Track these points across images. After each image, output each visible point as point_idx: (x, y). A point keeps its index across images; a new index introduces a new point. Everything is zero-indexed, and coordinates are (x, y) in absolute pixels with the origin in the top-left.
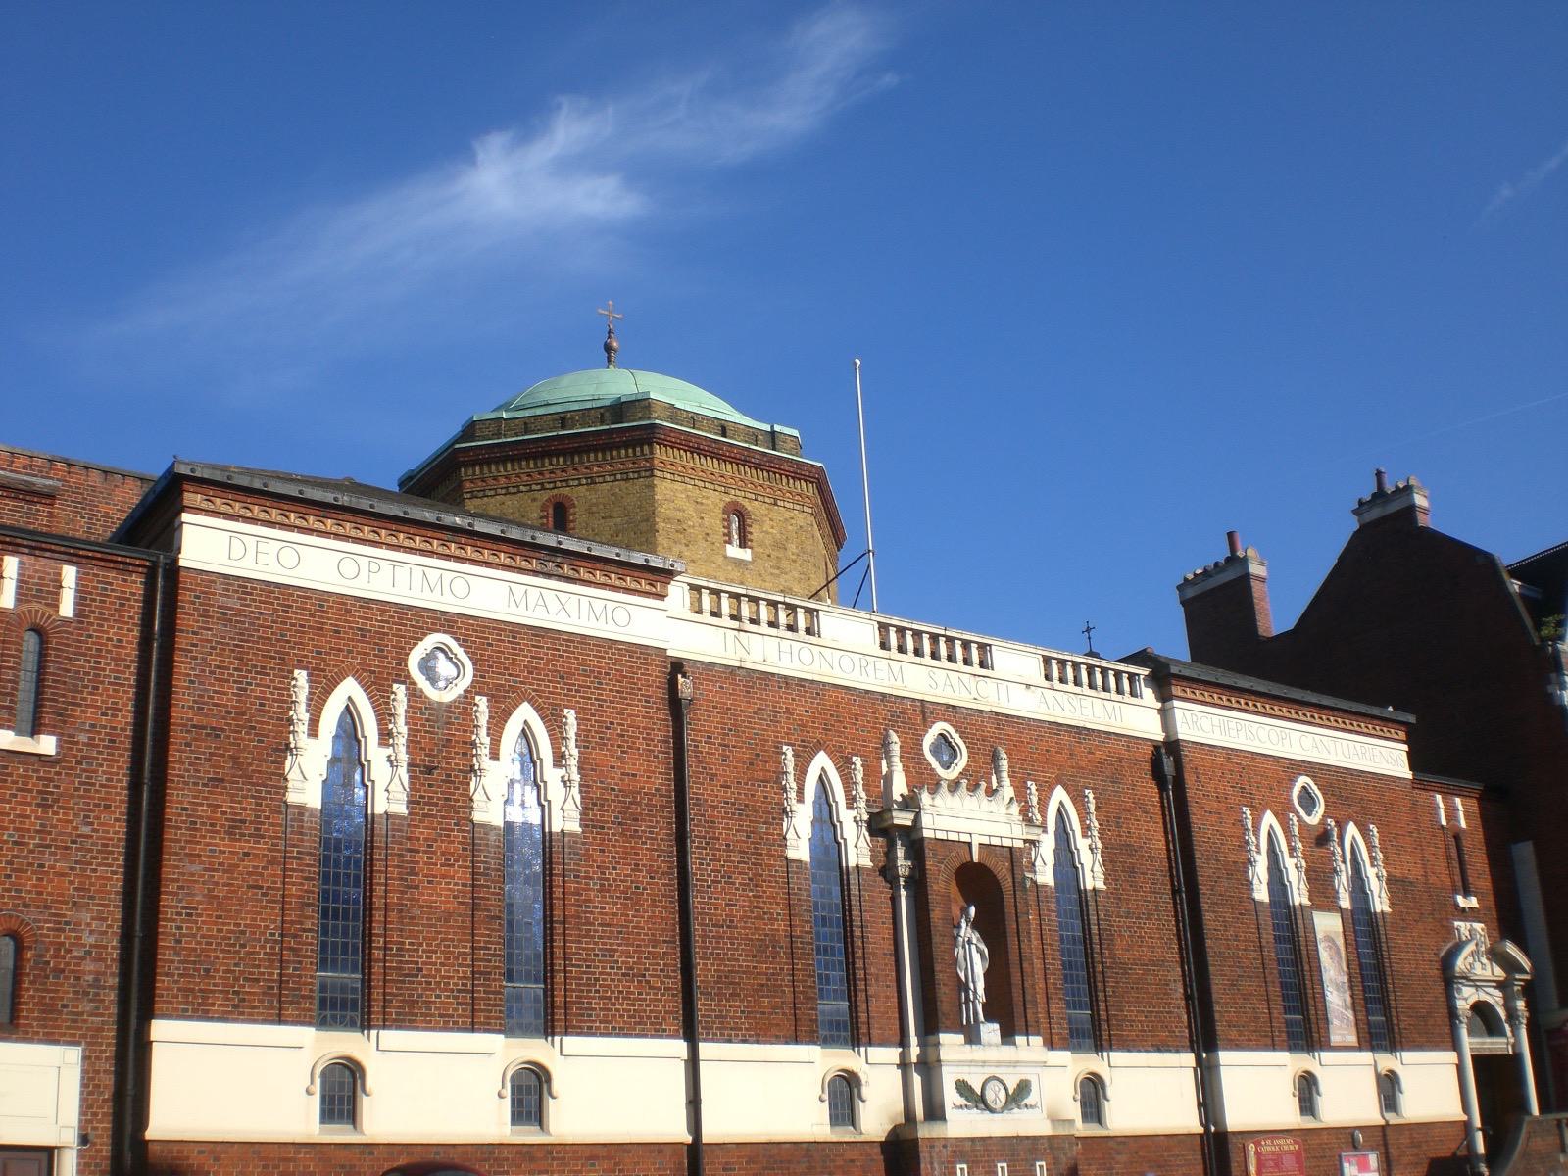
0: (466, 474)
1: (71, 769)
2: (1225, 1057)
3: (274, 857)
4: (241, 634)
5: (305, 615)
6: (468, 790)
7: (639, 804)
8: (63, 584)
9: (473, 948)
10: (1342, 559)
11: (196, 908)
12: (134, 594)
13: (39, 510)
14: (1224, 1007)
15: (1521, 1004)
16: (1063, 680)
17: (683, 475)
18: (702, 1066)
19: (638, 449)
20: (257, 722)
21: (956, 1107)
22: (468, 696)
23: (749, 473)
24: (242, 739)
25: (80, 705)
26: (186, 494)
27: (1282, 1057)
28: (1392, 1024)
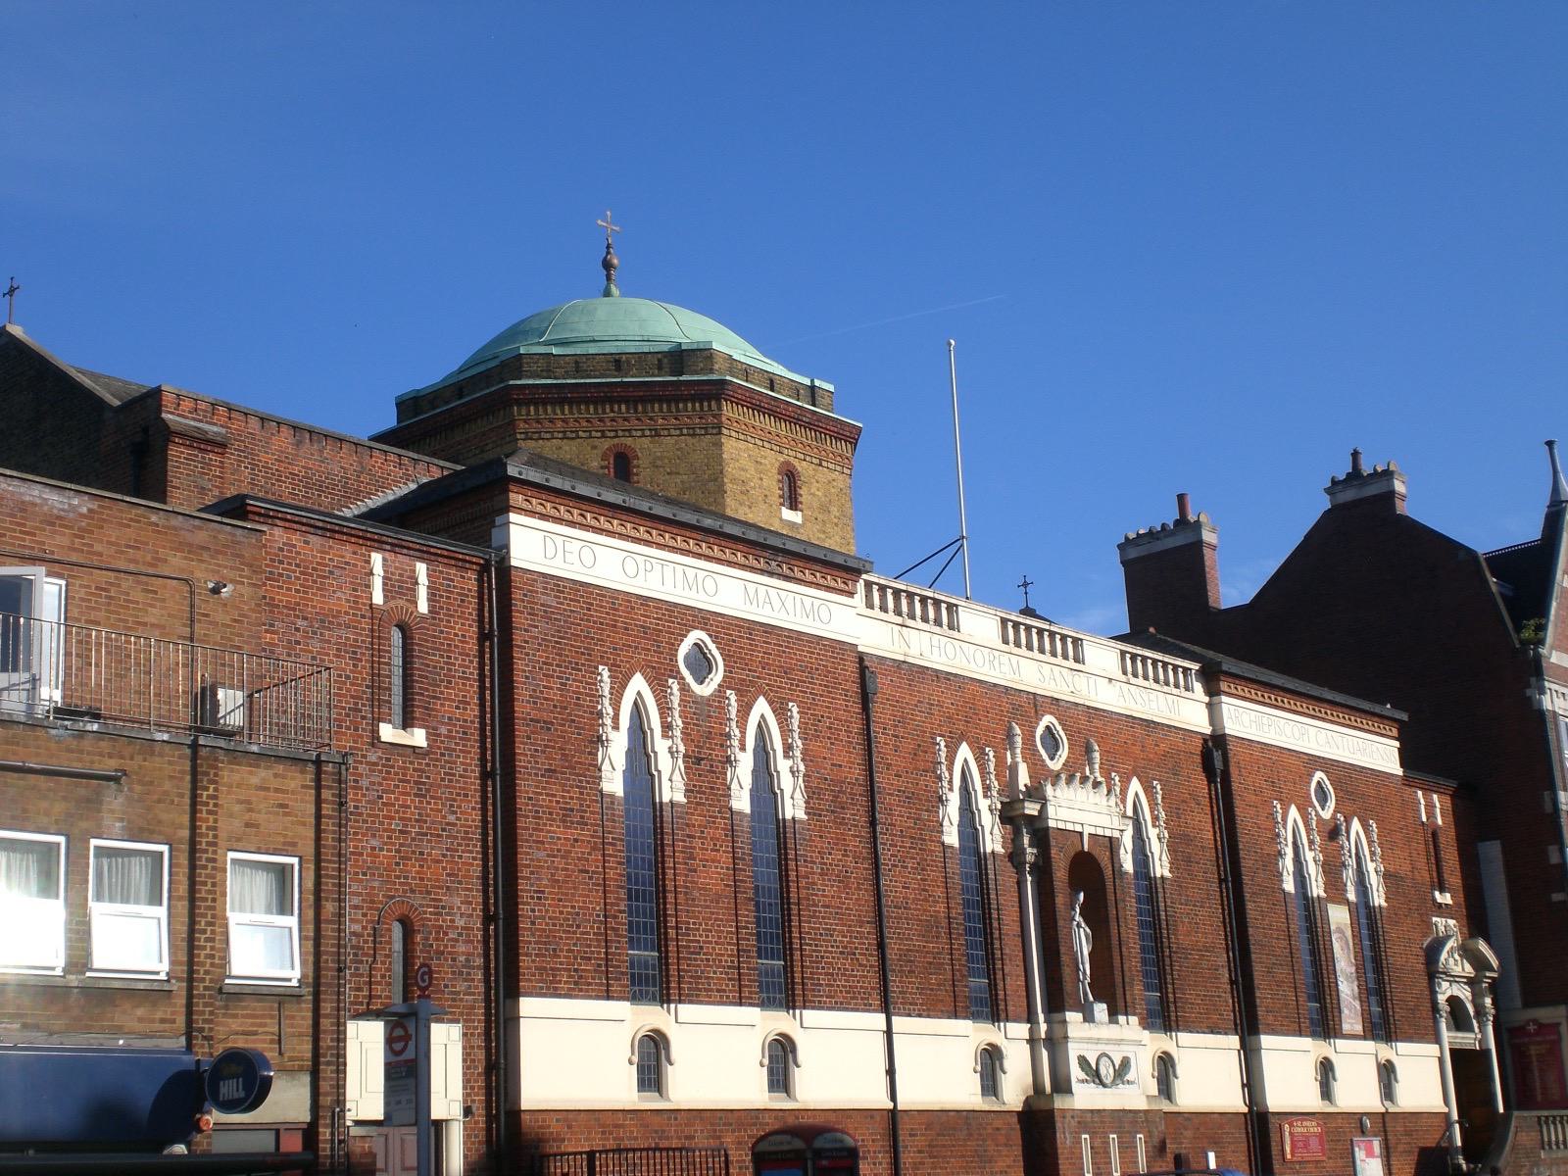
0: (520, 414)
1: (437, 760)
2: (1267, 1041)
3: (595, 843)
4: (559, 631)
5: (602, 612)
6: (725, 779)
7: (844, 793)
8: (374, 571)
9: (737, 927)
11: (543, 892)
12: (470, 590)
13: (211, 459)
14: (1263, 995)
15: (1488, 1001)
16: (1135, 675)
17: (746, 432)
19: (706, 404)
20: (576, 715)
21: (1082, 1081)
23: (801, 434)
24: (566, 732)
25: (439, 698)
26: (511, 494)
27: (1306, 1042)
28: (1388, 1016)
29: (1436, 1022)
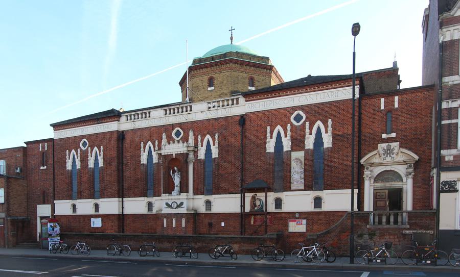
18: (246, 198)
22: (88, 148)
23: (214, 68)
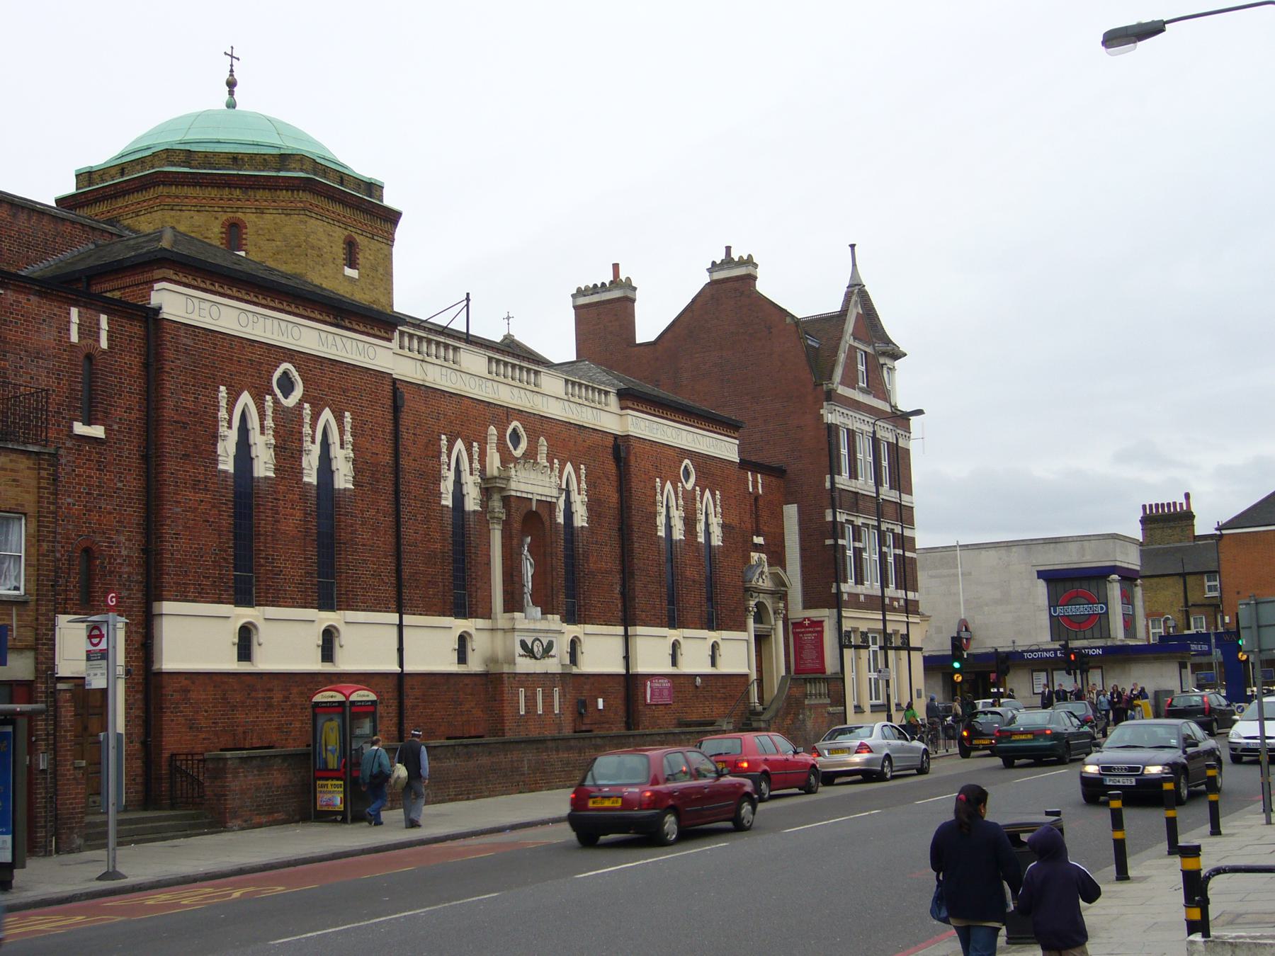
10: (693, 301)
14: (641, 601)
22: (300, 405)
23: (360, 217)
29: (746, 617)
